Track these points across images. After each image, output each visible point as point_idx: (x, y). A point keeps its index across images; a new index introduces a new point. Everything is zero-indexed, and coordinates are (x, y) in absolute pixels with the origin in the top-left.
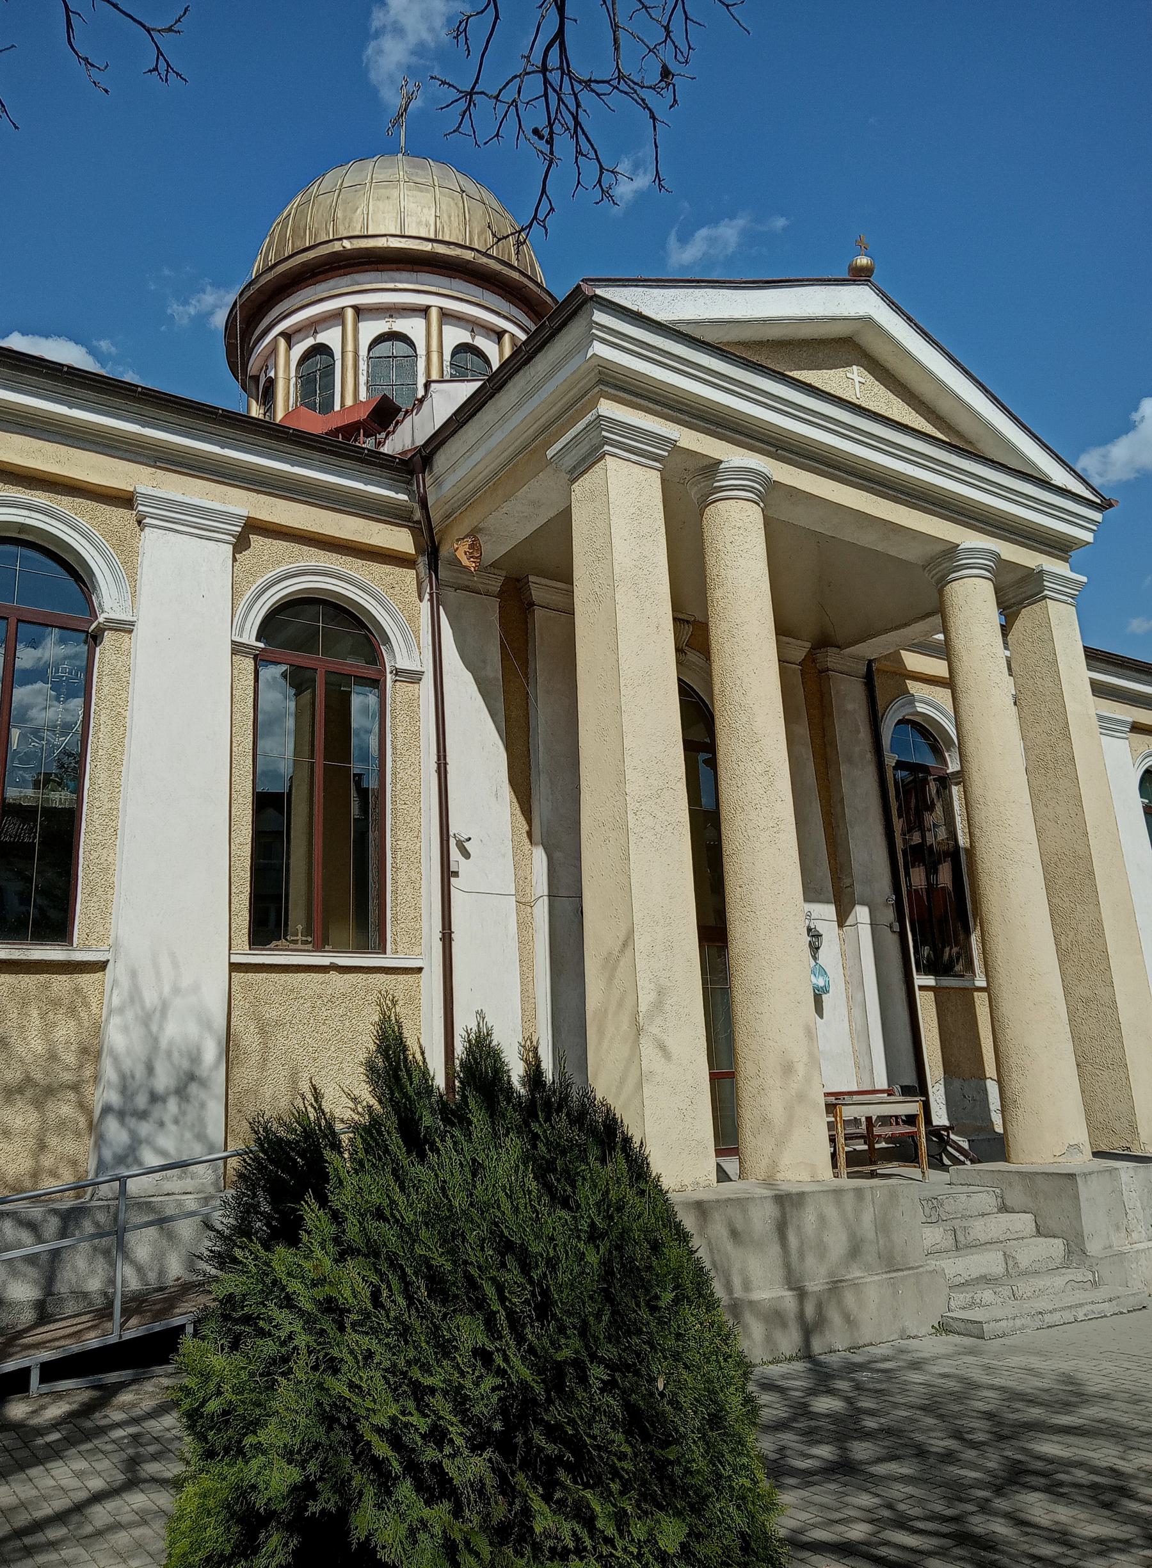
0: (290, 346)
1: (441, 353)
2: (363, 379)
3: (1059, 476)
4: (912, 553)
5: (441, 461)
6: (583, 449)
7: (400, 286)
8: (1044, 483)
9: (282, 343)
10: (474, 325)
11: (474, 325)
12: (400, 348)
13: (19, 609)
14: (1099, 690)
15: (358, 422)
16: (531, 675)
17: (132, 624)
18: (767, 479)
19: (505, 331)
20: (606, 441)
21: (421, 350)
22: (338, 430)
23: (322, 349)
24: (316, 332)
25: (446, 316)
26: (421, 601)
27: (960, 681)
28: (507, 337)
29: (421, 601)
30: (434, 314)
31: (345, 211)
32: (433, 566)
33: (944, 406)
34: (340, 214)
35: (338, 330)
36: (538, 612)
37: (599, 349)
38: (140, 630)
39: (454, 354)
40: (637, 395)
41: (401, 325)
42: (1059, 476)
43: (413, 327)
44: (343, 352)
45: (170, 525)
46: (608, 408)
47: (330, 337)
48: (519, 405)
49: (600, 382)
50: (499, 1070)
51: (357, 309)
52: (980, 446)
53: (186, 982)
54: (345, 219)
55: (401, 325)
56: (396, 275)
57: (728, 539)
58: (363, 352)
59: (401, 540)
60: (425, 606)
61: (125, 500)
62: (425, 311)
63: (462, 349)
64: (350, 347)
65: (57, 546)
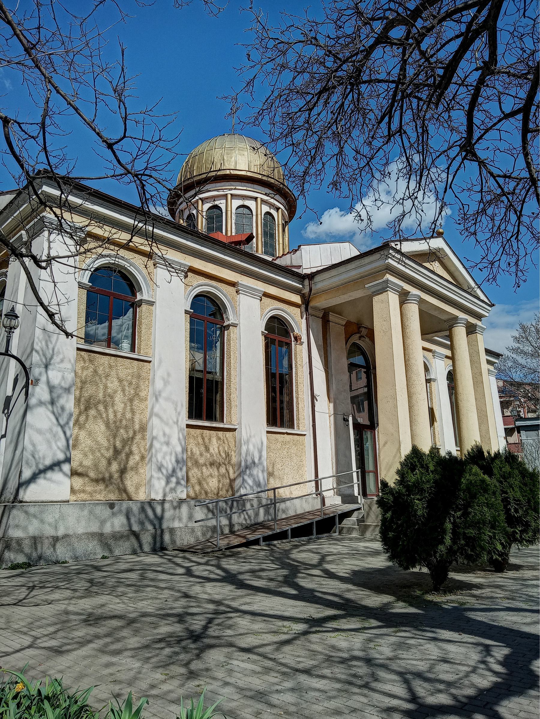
0: (203, 204)
1: (261, 215)
2: (233, 221)
3: (482, 297)
4: (444, 317)
5: (317, 278)
6: (380, 287)
7: (248, 189)
8: (479, 299)
9: (200, 202)
10: (271, 205)
11: (271, 205)
12: (246, 211)
13: (114, 294)
14: (489, 362)
15: (241, 241)
16: (328, 344)
17: (154, 302)
18: (403, 289)
19: (280, 208)
20: (388, 287)
21: (254, 213)
22: (232, 243)
23: (217, 207)
24: (214, 200)
25: (263, 201)
26: (302, 318)
27: (457, 357)
28: (280, 210)
29: (302, 318)
30: (259, 200)
31: (227, 157)
32: (307, 310)
33: (456, 274)
34: (225, 158)
35: (224, 201)
36: (331, 323)
37: (390, 261)
38: (242, 326)
39: (264, 215)
40: (394, 273)
41: (248, 203)
42: (482, 297)
43: (251, 204)
44: (227, 211)
45: (246, 293)
46: (388, 277)
47: (221, 204)
48: (355, 269)
49: (386, 269)
50: (483, 453)
51: (232, 195)
52: (463, 286)
53: (252, 435)
54: (228, 160)
55: (248, 203)
56: (247, 184)
57: (411, 315)
58: (234, 211)
59: (297, 299)
60: (304, 321)
61: (233, 284)
62: (256, 199)
63: (268, 213)
64: (229, 209)
65: (215, 298)
